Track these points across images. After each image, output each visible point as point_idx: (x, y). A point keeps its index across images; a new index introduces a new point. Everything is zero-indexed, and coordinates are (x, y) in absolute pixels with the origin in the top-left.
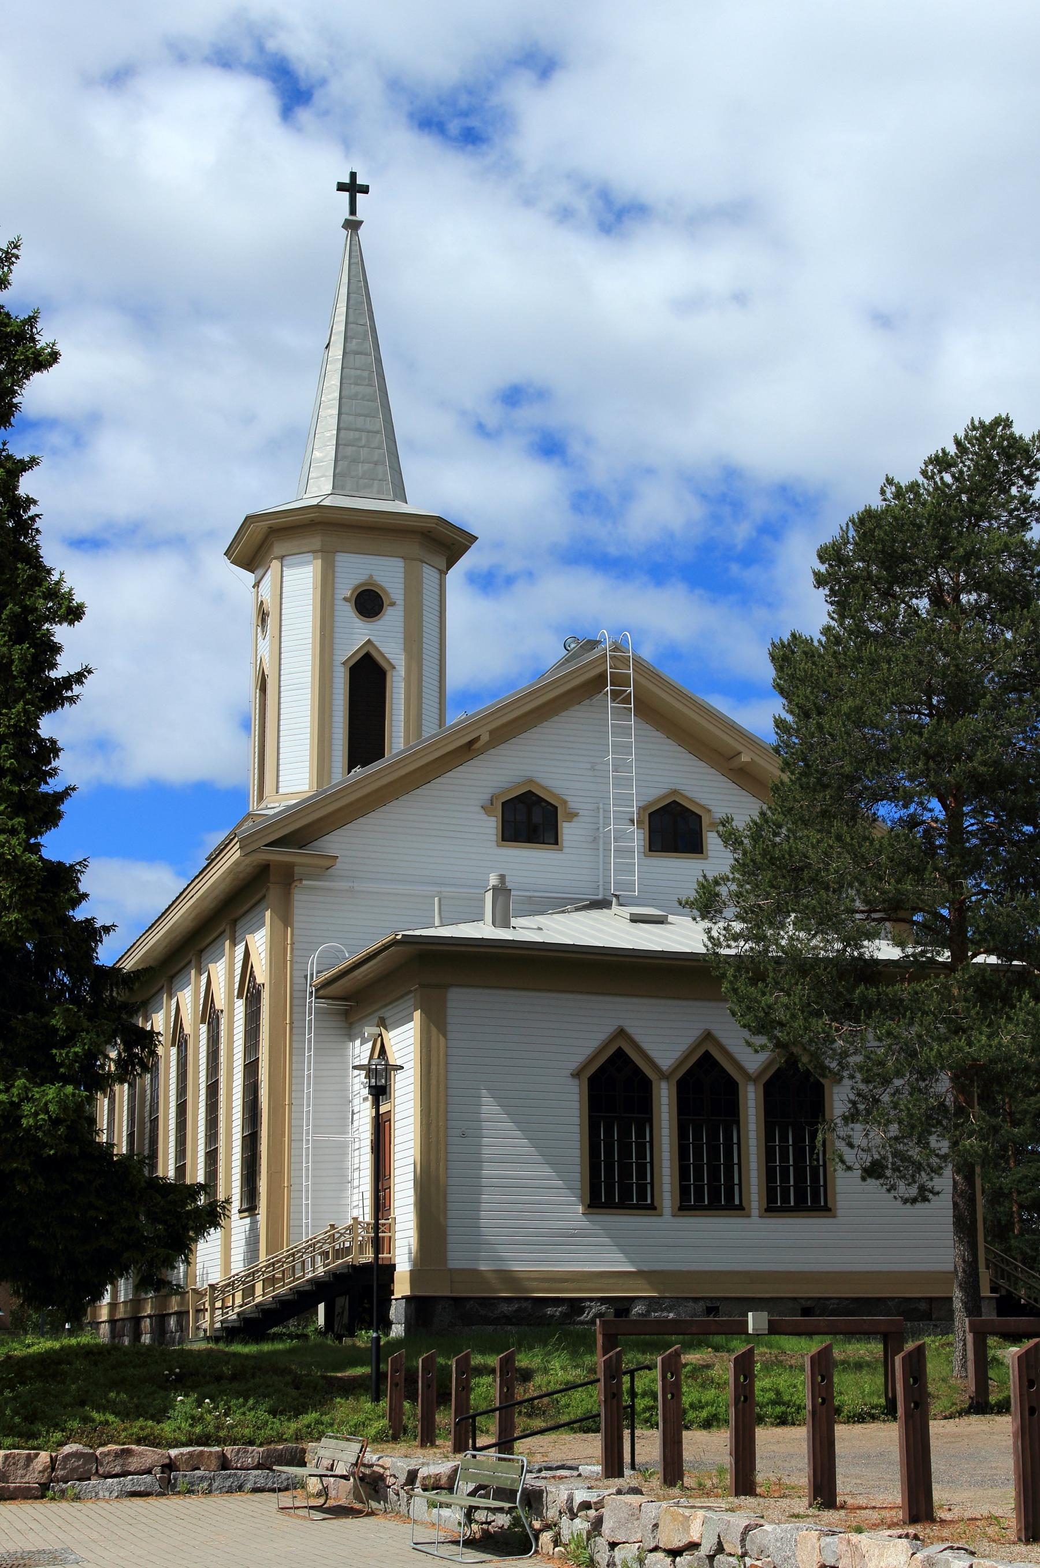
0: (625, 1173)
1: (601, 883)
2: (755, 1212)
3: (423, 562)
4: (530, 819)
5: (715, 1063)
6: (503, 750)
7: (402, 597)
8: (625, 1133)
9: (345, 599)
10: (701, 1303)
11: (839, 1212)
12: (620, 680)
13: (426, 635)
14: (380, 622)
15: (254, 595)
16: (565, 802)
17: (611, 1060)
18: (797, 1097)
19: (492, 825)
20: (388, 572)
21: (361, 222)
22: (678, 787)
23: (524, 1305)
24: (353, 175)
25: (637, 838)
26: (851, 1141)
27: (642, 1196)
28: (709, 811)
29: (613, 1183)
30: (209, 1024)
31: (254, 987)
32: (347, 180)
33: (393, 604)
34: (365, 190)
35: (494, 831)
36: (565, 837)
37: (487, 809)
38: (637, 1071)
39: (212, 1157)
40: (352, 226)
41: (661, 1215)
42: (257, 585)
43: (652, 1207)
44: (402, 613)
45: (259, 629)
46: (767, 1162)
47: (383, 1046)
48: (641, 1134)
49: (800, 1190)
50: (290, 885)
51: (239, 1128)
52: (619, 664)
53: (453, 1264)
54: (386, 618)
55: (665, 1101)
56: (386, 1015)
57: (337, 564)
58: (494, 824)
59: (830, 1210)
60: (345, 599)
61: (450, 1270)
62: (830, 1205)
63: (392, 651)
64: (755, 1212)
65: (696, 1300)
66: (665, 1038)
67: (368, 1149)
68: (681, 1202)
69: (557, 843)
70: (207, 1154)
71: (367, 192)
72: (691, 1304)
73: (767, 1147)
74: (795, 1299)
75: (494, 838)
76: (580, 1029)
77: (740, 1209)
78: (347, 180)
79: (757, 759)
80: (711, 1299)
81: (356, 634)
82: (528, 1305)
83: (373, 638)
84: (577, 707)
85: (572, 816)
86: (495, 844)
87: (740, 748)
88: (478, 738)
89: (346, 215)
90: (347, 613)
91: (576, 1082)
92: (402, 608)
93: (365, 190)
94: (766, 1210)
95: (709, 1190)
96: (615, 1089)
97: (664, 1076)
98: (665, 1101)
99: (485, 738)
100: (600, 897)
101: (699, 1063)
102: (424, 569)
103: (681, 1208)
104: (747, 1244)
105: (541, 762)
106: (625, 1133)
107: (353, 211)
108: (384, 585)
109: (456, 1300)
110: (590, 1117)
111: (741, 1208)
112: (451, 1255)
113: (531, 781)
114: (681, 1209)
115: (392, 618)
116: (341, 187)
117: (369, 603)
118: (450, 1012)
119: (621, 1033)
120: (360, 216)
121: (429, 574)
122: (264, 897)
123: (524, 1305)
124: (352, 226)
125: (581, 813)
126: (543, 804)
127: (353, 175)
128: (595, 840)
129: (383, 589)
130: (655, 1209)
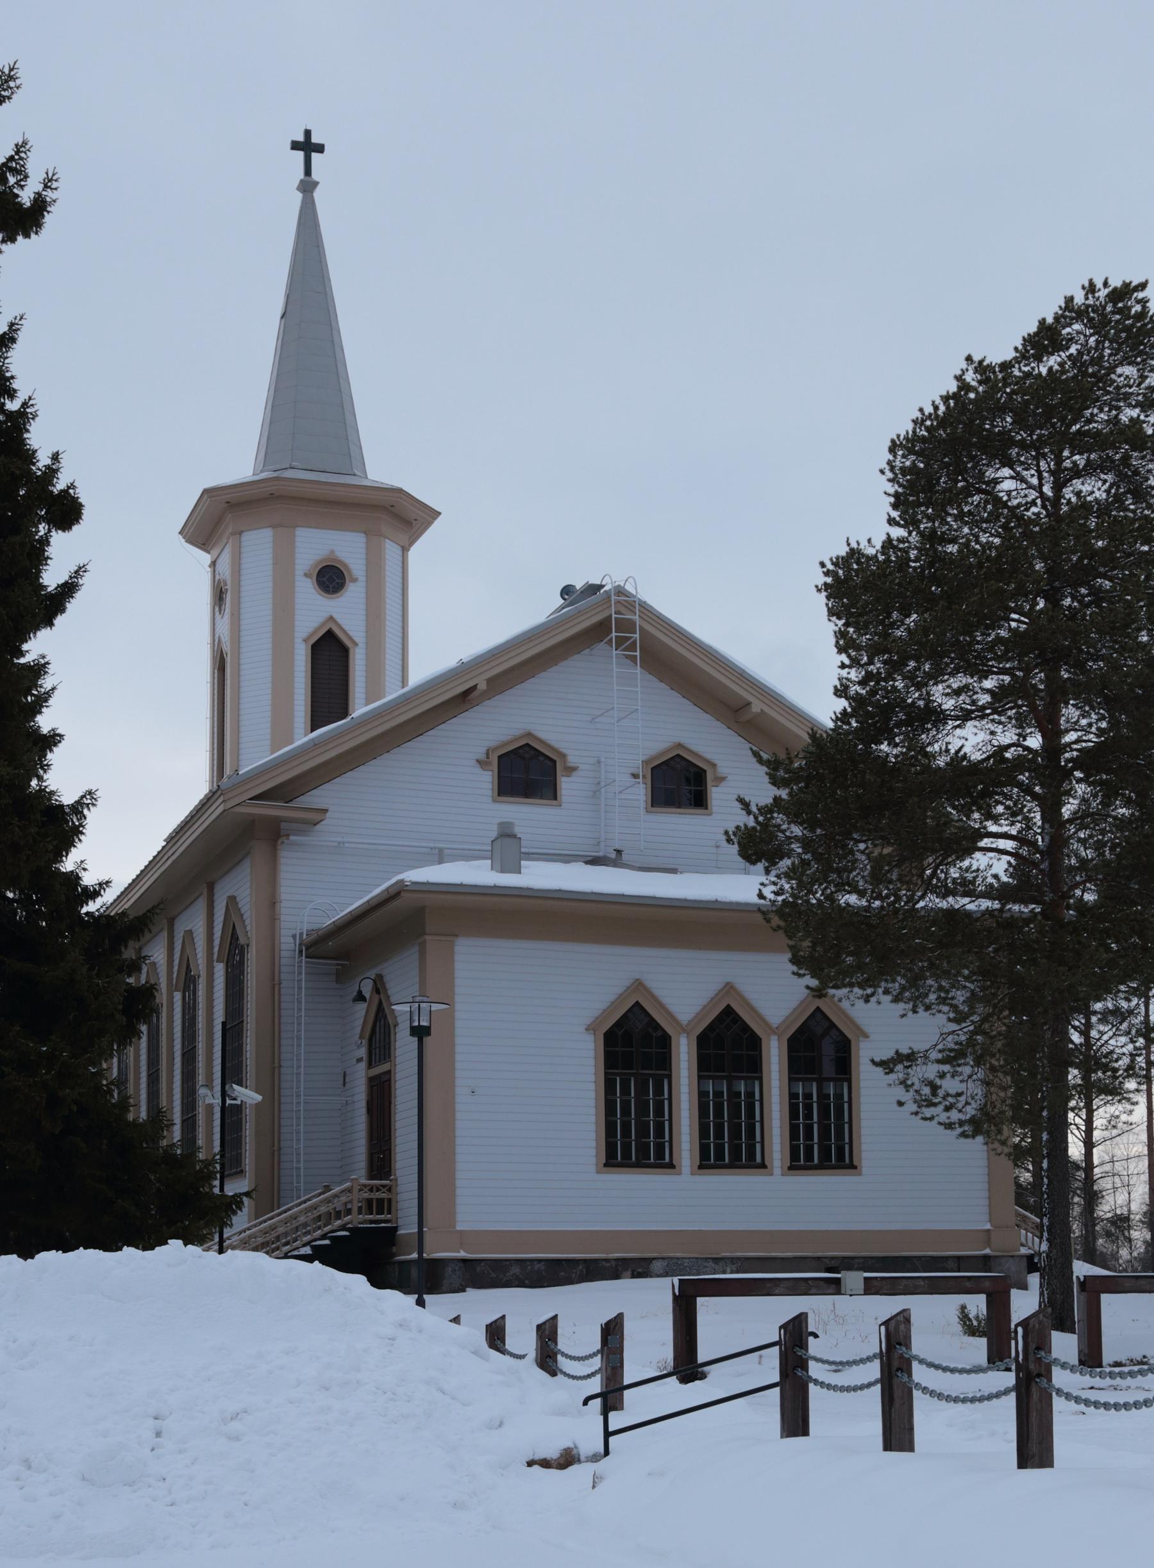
2: (777, 1170)
4: (527, 772)
5: (737, 1019)
6: (497, 701)
7: (364, 573)
8: (642, 1089)
11: (864, 1170)
12: (626, 626)
13: (387, 609)
14: (341, 599)
16: (563, 756)
18: (822, 1052)
19: (487, 780)
20: (347, 546)
21: (317, 183)
22: (677, 740)
24: (308, 133)
25: (641, 792)
26: (876, 1100)
27: (660, 1154)
29: (632, 1139)
32: (300, 138)
33: (355, 580)
34: (320, 149)
35: (490, 786)
37: (482, 764)
40: (308, 186)
41: (680, 1174)
42: (213, 564)
45: (217, 609)
46: (791, 1119)
47: (380, 1003)
48: (659, 1091)
49: (825, 1144)
50: (276, 841)
52: (623, 610)
58: (489, 779)
59: (855, 1167)
60: (306, 575)
62: (855, 1163)
63: (353, 626)
64: (777, 1170)
66: (684, 990)
67: (364, 1111)
68: (701, 1160)
69: (555, 798)
73: (790, 1104)
75: (489, 793)
76: (596, 980)
78: (300, 138)
79: (767, 710)
81: (313, 610)
83: (335, 616)
84: (576, 657)
86: (490, 799)
87: (750, 698)
88: (474, 688)
90: (306, 591)
92: (364, 584)
93: (320, 149)
94: (606, 1165)
95: (730, 1146)
96: (632, 1046)
97: (684, 1029)
99: (482, 686)
100: (601, 854)
101: (720, 1018)
103: (791, 1168)
104: (774, 1201)
105: (536, 714)
106: (642, 1089)
107: (308, 171)
108: (347, 561)
110: (606, 1073)
111: (763, 1166)
112: (459, 1217)
113: (529, 734)
114: (701, 1167)
115: (354, 593)
116: (295, 146)
117: (331, 578)
120: (315, 175)
121: (391, 550)
124: (308, 186)
125: (581, 767)
126: (541, 758)
127: (308, 133)
129: (345, 565)
130: (855, 1167)
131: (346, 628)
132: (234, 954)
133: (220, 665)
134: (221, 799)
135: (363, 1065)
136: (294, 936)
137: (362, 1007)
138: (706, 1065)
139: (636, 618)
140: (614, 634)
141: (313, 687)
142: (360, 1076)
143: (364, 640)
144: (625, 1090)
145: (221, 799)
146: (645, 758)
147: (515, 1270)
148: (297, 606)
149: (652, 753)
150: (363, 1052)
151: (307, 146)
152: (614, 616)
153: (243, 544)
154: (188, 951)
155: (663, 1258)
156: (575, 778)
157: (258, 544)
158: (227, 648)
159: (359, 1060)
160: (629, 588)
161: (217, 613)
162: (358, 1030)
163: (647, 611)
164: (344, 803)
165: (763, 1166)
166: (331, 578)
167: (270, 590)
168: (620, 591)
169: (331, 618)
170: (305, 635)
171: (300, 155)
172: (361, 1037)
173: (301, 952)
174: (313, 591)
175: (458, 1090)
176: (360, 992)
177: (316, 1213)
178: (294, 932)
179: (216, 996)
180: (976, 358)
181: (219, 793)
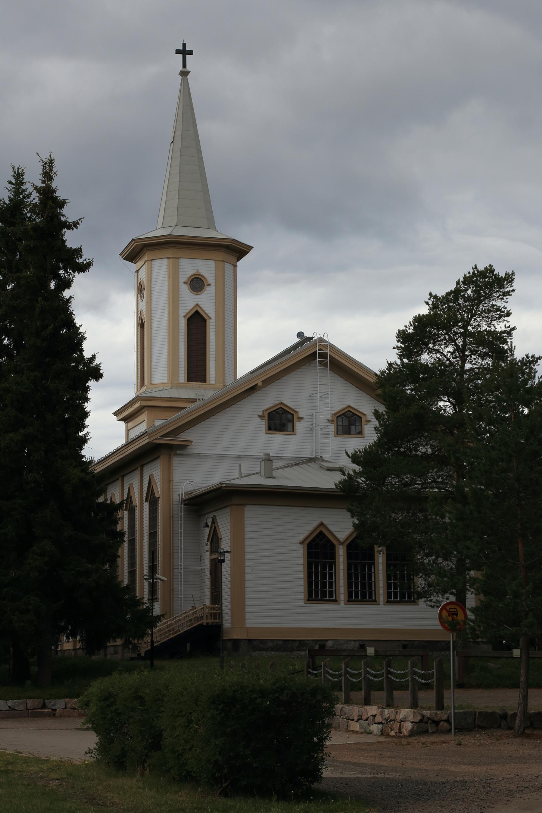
0: (324, 585)
1: (314, 450)
2: (382, 603)
3: (224, 262)
4: (280, 420)
7: (214, 281)
9: (184, 283)
10: (357, 642)
12: (323, 356)
15: (136, 276)
17: (317, 536)
19: (263, 424)
20: (206, 267)
21: (189, 72)
23: (279, 642)
24: (184, 45)
25: (331, 429)
28: (365, 415)
29: (319, 588)
30: (129, 511)
31: (153, 498)
33: (209, 285)
34: (191, 53)
35: (264, 426)
36: (297, 428)
38: (329, 541)
39: (132, 573)
40: (184, 74)
43: (336, 601)
44: (214, 290)
45: (139, 295)
46: (387, 581)
47: (215, 528)
51: (147, 562)
53: (248, 625)
54: (206, 292)
55: (341, 554)
56: (216, 515)
57: (180, 264)
60: (184, 283)
61: (247, 628)
64: (382, 603)
65: (354, 641)
70: (129, 572)
71: (192, 54)
72: (353, 643)
74: (400, 641)
75: (264, 429)
76: (303, 523)
77: (375, 602)
80: (362, 640)
81: (189, 301)
82: (281, 642)
83: (199, 303)
85: (300, 419)
89: (181, 68)
90: (185, 290)
91: (302, 546)
93: (191, 53)
94: (308, 600)
95: (361, 593)
96: (319, 549)
98: (341, 554)
99: (260, 384)
100: (314, 456)
102: (226, 266)
107: (184, 66)
109: (250, 641)
111: (375, 601)
112: (247, 621)
114: (348, 601)
115: (209, 292)
116: (178, 52)
117: (197, 284)
118: (246, 515)
119: (322, 524)
121: (228, 267)
122: (159, 457)
123: (279, 642)
124: (184, 74)
127: (184, 45)
128: (311, 429)
131: (204, 309)
132: (153, 500)
133: (141, 325)
134: (147, 437)
135: (208, 553)
136: (179, 495)
137: (208, 530)
138: (350, 556)
139: (328, 352)
140: (318, 360)
141: (188, 370)
142: (207, 558)
143: (214, 315)
144: (316, 568)
145: (147, 437)
146: (334, 412)
147: (270, 644)
148: (180, 299)
149: (338, 410)
150: (208, 548)
151: (184, 52)
152: (318, 351)
153: (153, 266)
154: (131, 492)
155: (332, 640)
156: (302, 422)
157: (160, 268)
158: (145, 319)
159: (207, 551)
160: (325, 338)
161: (140, 300)
162: (207, 537)
163: (332, 347)
164: (201, 439)
165: (375, 601)
166: (197, 284)
167: (167, 290)
168: (321, 340)
169: (197, 305)
170: (184, 314)
171: (180, 56)
172: (208, 541)
173: (182, 502)
174: (188, 291)
175: (246, 568)
176: (207, 523)
177: (189, 619)
178: (178, 493)
179: (144, 517)
180: (434, 294)
181: (147, 434)
